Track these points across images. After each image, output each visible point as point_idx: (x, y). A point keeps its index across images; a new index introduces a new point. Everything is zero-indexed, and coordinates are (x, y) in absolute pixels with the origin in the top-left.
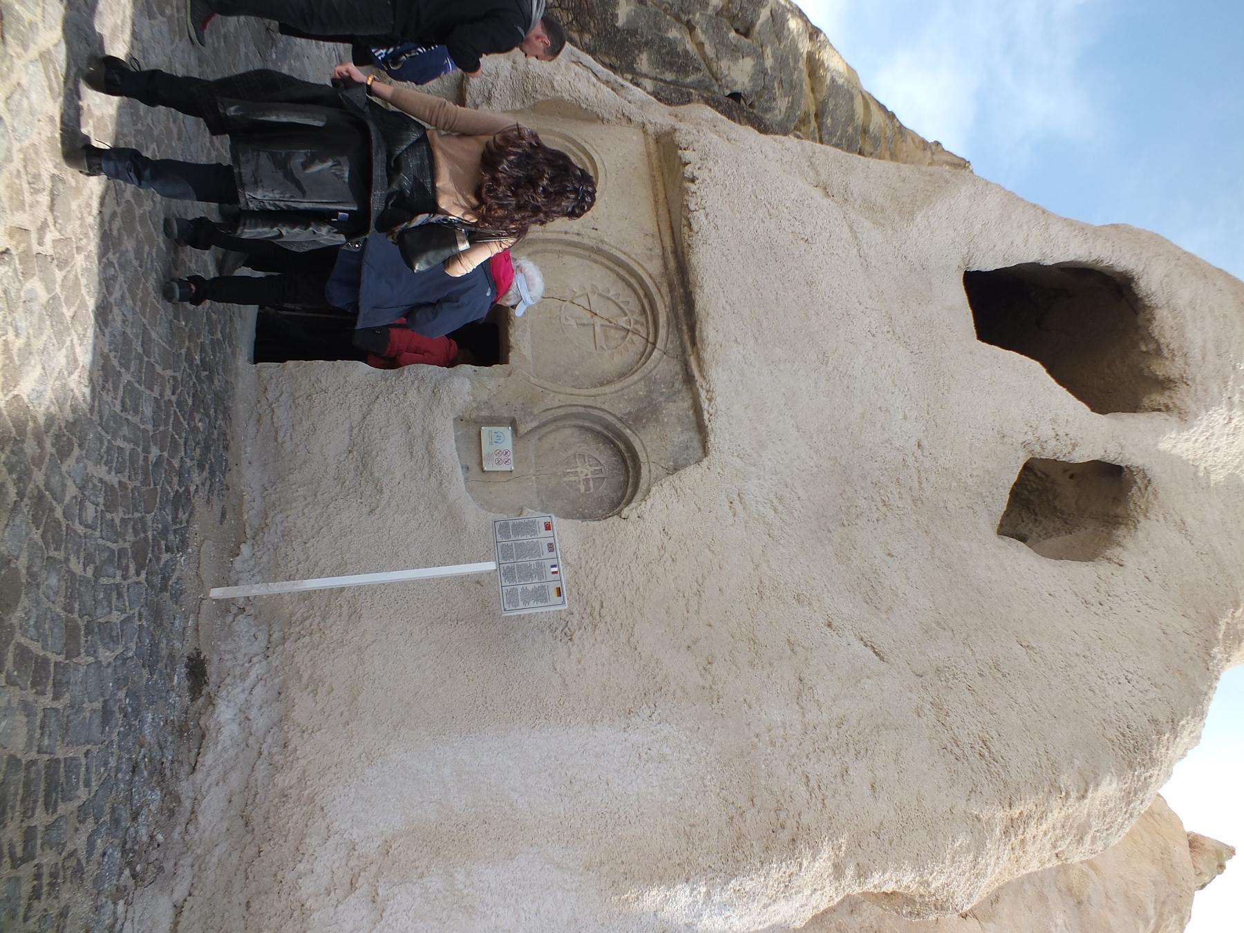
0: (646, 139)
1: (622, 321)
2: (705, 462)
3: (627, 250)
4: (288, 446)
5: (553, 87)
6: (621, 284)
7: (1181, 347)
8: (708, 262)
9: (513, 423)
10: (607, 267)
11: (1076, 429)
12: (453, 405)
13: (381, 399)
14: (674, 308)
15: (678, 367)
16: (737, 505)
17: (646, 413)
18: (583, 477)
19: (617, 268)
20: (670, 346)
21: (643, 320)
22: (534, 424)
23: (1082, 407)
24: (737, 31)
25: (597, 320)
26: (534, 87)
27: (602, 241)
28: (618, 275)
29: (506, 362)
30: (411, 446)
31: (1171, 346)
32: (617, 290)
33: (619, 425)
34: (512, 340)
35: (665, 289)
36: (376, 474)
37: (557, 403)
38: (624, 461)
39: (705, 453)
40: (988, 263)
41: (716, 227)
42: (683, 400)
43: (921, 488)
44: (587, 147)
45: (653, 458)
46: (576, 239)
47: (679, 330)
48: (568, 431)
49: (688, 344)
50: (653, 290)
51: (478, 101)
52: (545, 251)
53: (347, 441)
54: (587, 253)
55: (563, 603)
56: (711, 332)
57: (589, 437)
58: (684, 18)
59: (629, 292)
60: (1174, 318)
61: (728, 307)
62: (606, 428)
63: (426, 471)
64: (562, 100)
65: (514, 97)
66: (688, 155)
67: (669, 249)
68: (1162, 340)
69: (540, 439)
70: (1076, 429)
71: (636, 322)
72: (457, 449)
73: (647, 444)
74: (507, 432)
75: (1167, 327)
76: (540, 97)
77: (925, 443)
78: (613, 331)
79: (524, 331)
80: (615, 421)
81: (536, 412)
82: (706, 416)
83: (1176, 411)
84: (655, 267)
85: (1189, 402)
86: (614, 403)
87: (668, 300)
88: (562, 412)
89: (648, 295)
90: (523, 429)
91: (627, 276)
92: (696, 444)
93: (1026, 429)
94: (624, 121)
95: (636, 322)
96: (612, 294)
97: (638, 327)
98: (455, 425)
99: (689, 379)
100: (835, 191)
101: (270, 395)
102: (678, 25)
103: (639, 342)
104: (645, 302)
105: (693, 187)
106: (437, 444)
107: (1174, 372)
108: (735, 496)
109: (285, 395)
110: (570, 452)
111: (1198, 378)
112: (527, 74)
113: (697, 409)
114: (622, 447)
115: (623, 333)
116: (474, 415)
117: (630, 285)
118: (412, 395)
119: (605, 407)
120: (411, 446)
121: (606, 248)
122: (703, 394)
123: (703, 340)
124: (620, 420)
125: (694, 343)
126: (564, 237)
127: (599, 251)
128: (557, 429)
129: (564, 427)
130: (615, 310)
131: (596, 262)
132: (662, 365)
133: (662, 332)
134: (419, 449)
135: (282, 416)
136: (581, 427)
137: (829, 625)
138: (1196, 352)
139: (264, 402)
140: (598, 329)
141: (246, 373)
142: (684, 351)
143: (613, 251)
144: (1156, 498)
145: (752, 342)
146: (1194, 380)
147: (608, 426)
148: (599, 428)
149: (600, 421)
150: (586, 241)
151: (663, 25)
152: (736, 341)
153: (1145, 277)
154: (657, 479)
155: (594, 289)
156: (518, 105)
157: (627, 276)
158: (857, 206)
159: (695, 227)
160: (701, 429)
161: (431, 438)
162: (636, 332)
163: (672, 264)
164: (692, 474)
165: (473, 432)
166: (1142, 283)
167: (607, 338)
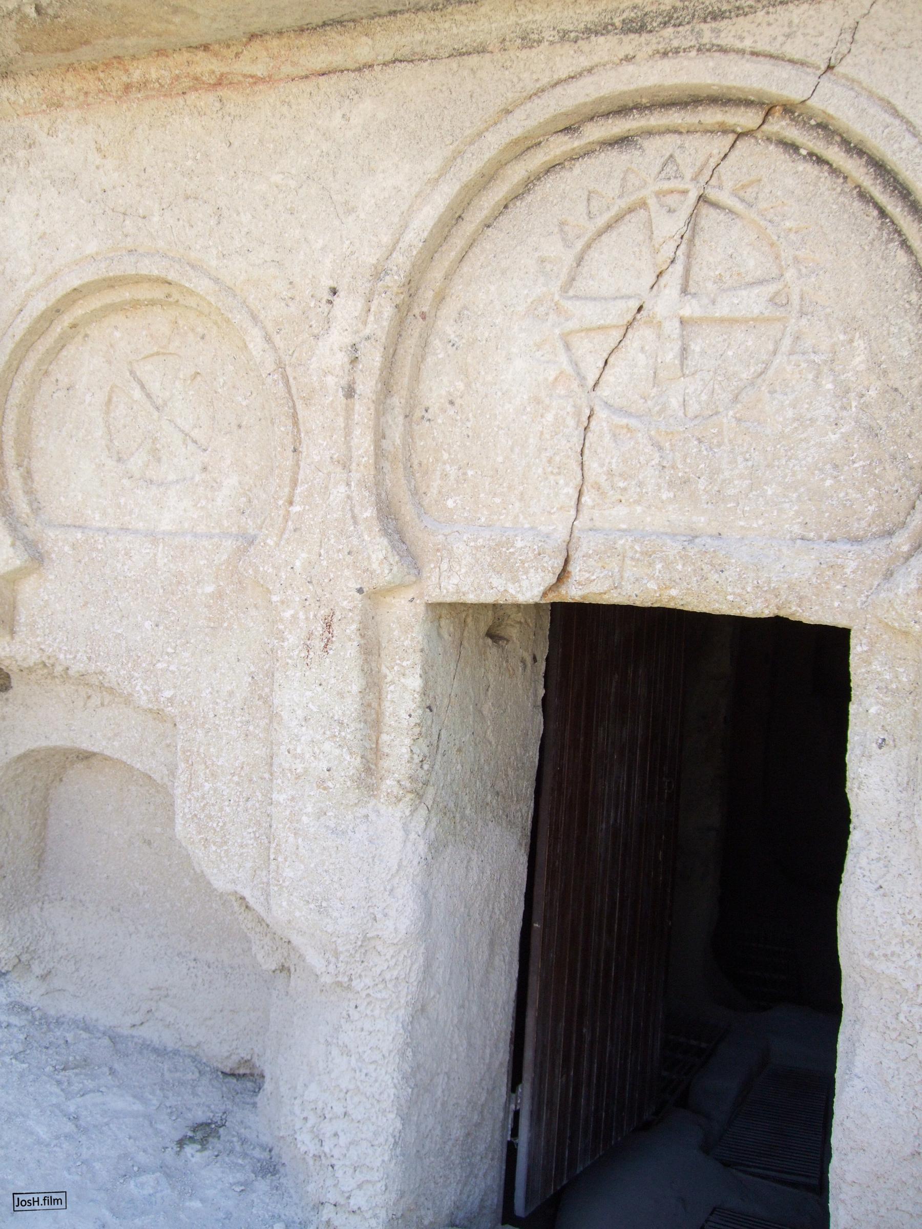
19: (468, 227)
27: (378, 273)
29: (834, 641)
54: (416, 328)
103: (758, 162)
117: (529, 184)
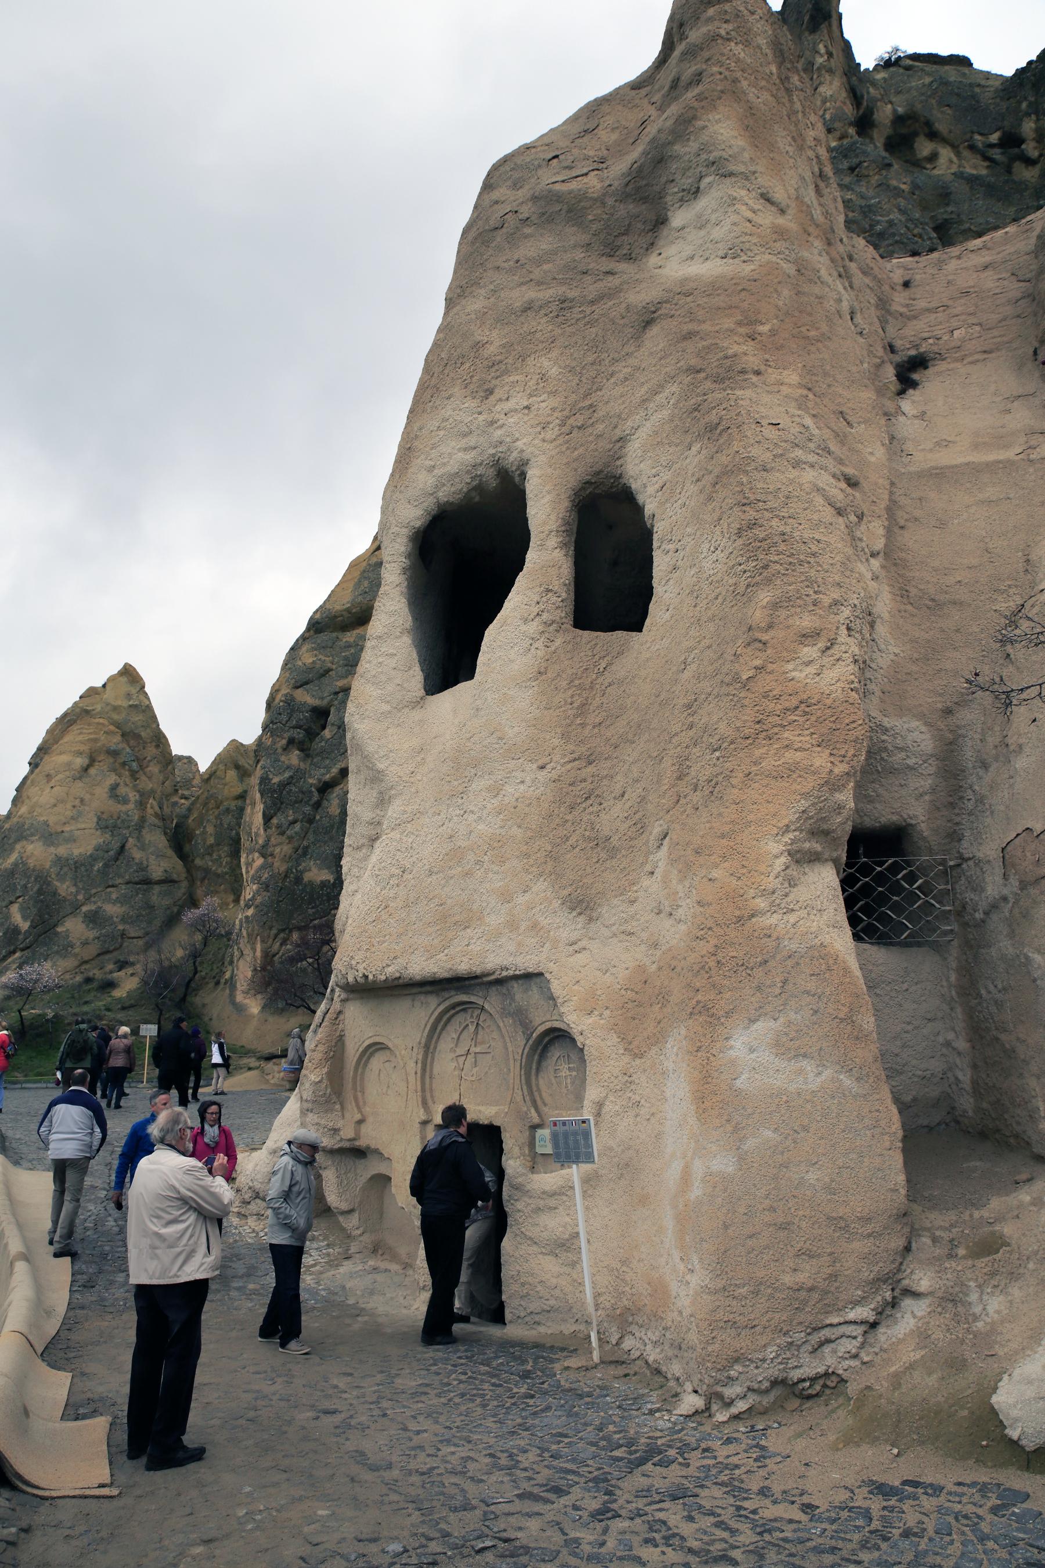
0: (352, 999)
1: (472, 1028)
2: (547, 975)
3: (424, 1023)
4: (552, 1302)
5: (320, 1082)
6: (448, 1028)
7: (468, 472)
8: (419, 967)
9: (534, 1127)
10: (439, 1038)
11: (546, 566)
12: (523, 1174)
13: (523, 1229)
14: (457, 989)
15: (494, 988)
16: (576, 947)
17: (521, 1018)
18: (568, 1073)
19: (439, 1028)
20: (480, 994)
21: (470, 1011)
22: (533, 1110)
23: (521, 581)
24: (324, 727)
25: (473, 1049)
26: (321, 1096)
27: (420, 1043)
28: (443, 1029)
30: (550, 1208)
31: (469, 481)
32: (445, 1044)
33: (531, 1042)
34: (486, 1122)
35: (446, 994)
36: (567, 1236)
37: (520, 1093)
38: (557, 1037)
39: (541, 974)
40: (416, 678)
41: (395, 958)
42: (513, 987)
43: (579, 758)
44: (361, 1050)
45: (548, 1017)
46: (419, 1065)
47: (470, 986)
48: (541, 1082)
49: (477, 981)
50: (447, 1003)
51: (338, 1138)
52: (431, 1090)
53: (550, 1257)
54: (430, 1055)
55: (589, 1120)
56: (463, 967)
57: (544, 1064)
58: (316, 796)
59: (453, 1020)
60: (444, 485)
61: (446, 951)
62: (535, 1051)
63: (565, 1198)
64: (328, 1073)
65: (332, 1110)
66: (351, 979)
67: (419, 989)
68: (465, 490)
69: (545, 1105)
70: (546, 566)
71: (472, 1017)
72: (552, 1172)
73: (542, 1021)
74: (540, 1132)
75: (453, 489)
76: (329, 1090)
77: (540, 763)
78: (479, 1037)
79: (480, 1111)
80: (528, 1046)
81: (525, 1109)
82: (517, 972)
83: (522, 468)
84: (433, 1001)
85: (511, 459)
86: (518, 1045)
87: (453, 993)
88: (525, 1087)
89: (453, 1006)
90: (536, 1120)
91: (442, 1023)
92: (538, 980)
93: (533, 650)
94: (341, 1017)
95: (472, 1017)
96: (455, 1036)
97: (475, 1015)
98: (537, 1173)
99: (500, 982)
100: (374, 833)
101: (522, 1314)
102: (325, 803)
104: (458, 1009)
105: (371, 977)
106: (547, 1188)
107: (491, 472)
108: (571, 948)
109: (522, 1303)
110: (553, 1081)
111: (492, 451)
112: (314, 1102)
113: (516, 978)
114: (547, 1039)
115: (480, 1028)
116: (529, 1158)
117: (449, 1020)
118: (519, 1205)
119: (520, 1052)
120: (550, 1208)
121: (423, 1041)
122: (504, 973)
123: (469, 973)
124: (528, 1041)
125: (476, 977)
126: (419, 1075)
127: (427, 1047)
128: (539, 1090)
129: (537, 1085)
130: (465, 1033)
131: (435, 1048)
132: (492, 1003)
133: (473, 999)
134: (552, 1202)
135: (533, 1306)
136: (538, 1070)
137: (653, 873)
138: (469, 457)
139: (527, 1319)
140: (478, 1050)
141: (512, 1331)
142: (483, 984)
143: (425, 1034)
144: (601, 471)
145: (468, 930)
146: (493, 455)
147: (533, 1049)
148: (536, 1057)
149: (530, 1056)
150: (420, 1057)
151: (325, 821)
152: (467, 945)
153: (412, 524)
154: (561, 1015)
155: (453, 1050)
156: (338, 1107)
157: (442, 1023)
158: (382, 813)
159: (397, 975)
160: (528, 976)
161: (544, 1193)
162: (478, 1016)
163: (428, 988)
164: (556, 987)
165: (539, 1159)
166: (418, 524)
167: (483, 1043)
